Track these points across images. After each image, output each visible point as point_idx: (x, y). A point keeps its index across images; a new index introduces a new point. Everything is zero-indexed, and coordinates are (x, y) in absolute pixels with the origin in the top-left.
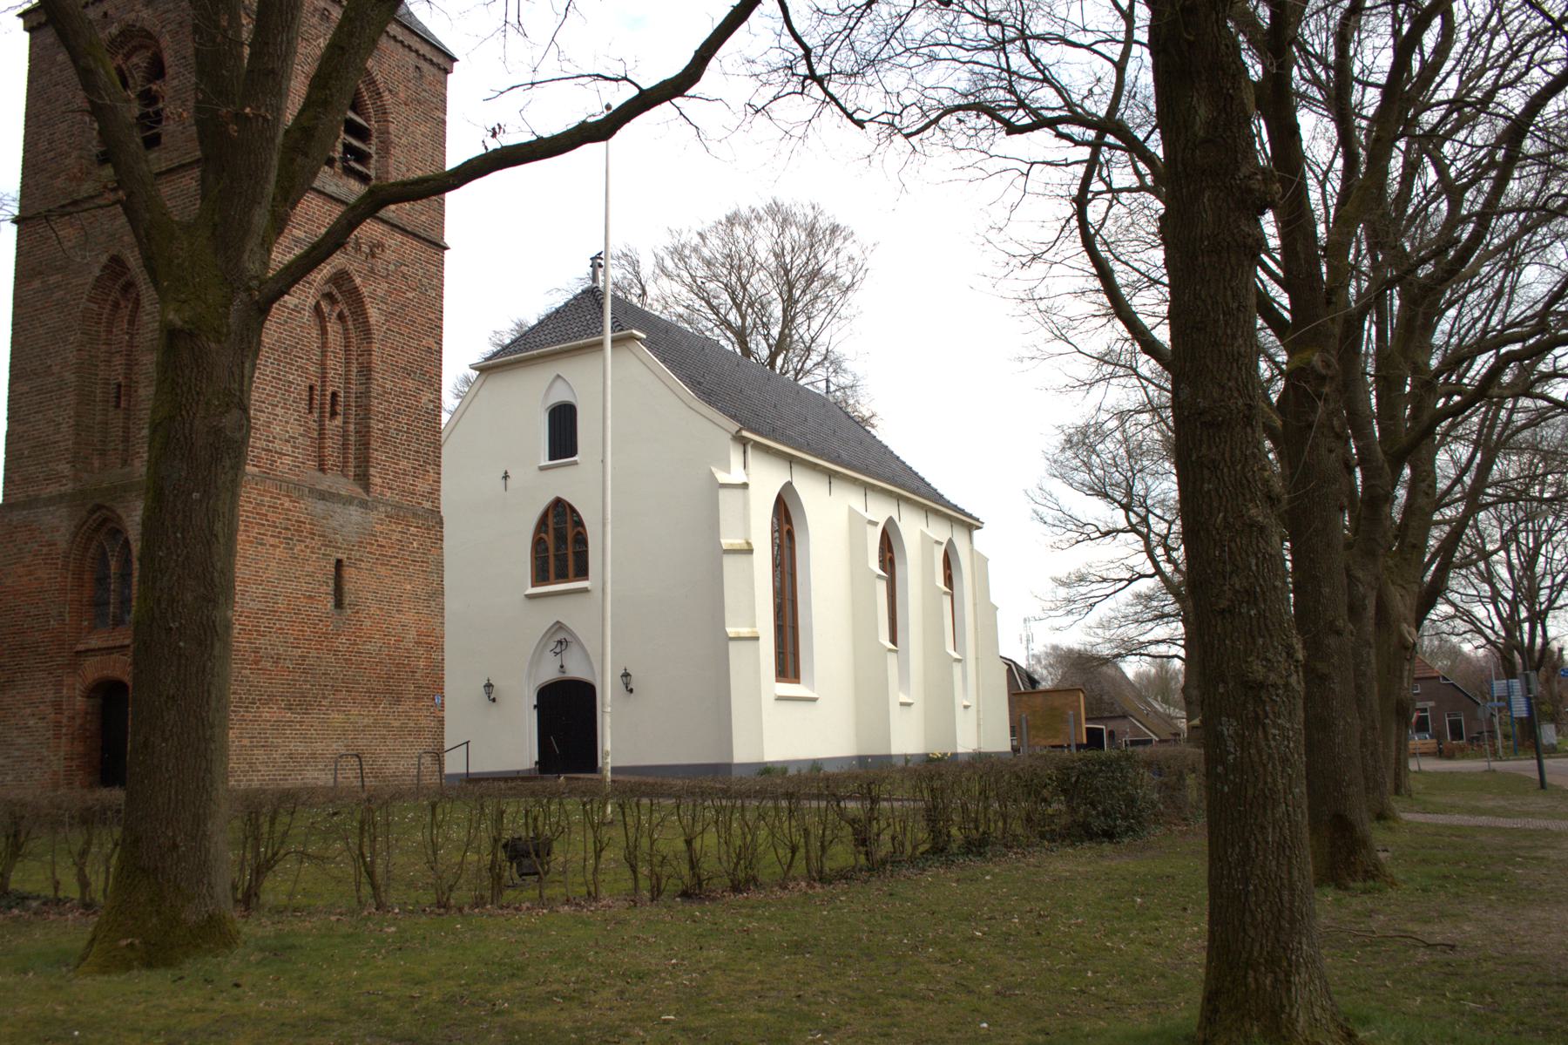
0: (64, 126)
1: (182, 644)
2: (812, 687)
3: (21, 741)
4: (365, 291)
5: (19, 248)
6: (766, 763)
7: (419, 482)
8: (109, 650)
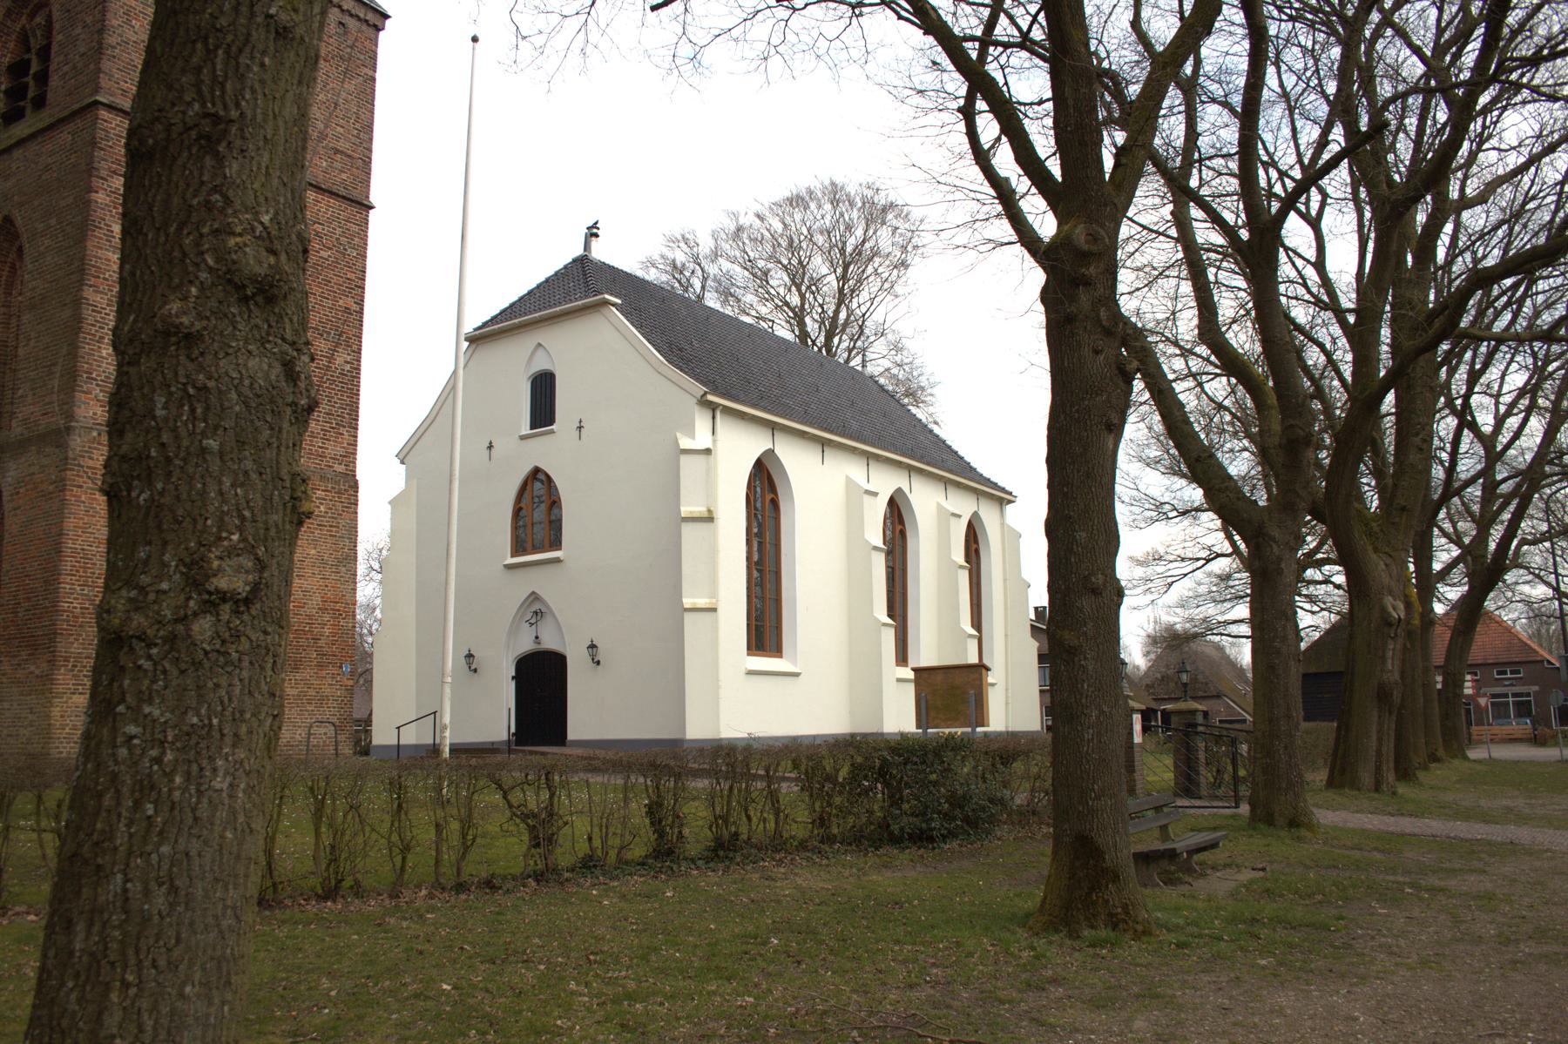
2: (794, 662)
6: (721, 739)
7: (330, 446)
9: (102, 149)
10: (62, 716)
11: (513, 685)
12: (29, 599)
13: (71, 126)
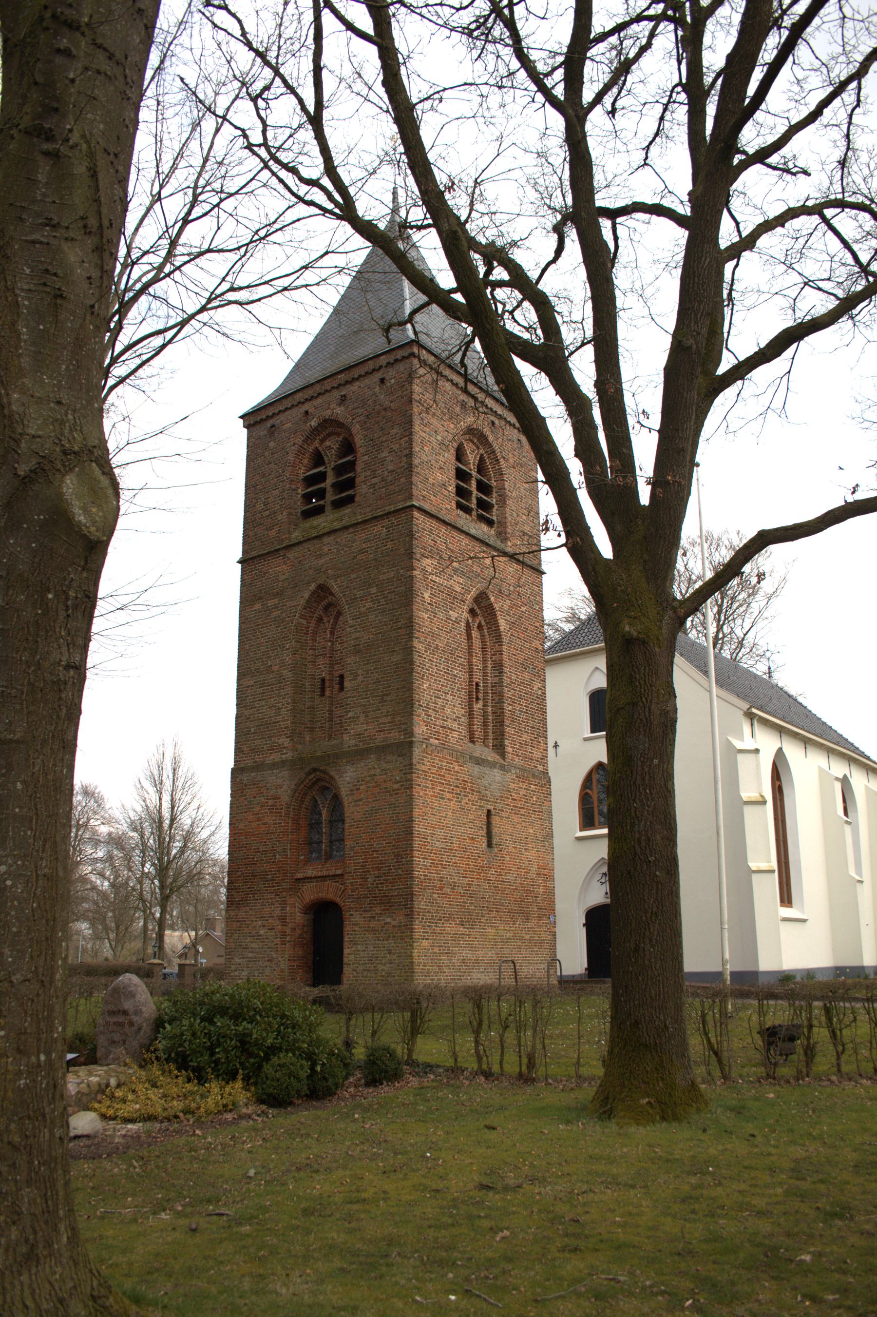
0: (276, 492)
1: (658, 873)
2: (802, 910)
3: (253, 945)
4: (496, 606)
5: (243, 580)
6: (784, 971)
8: (324, 878)
11: (584, 930)
12: (378, 869)
13: (386, 522)
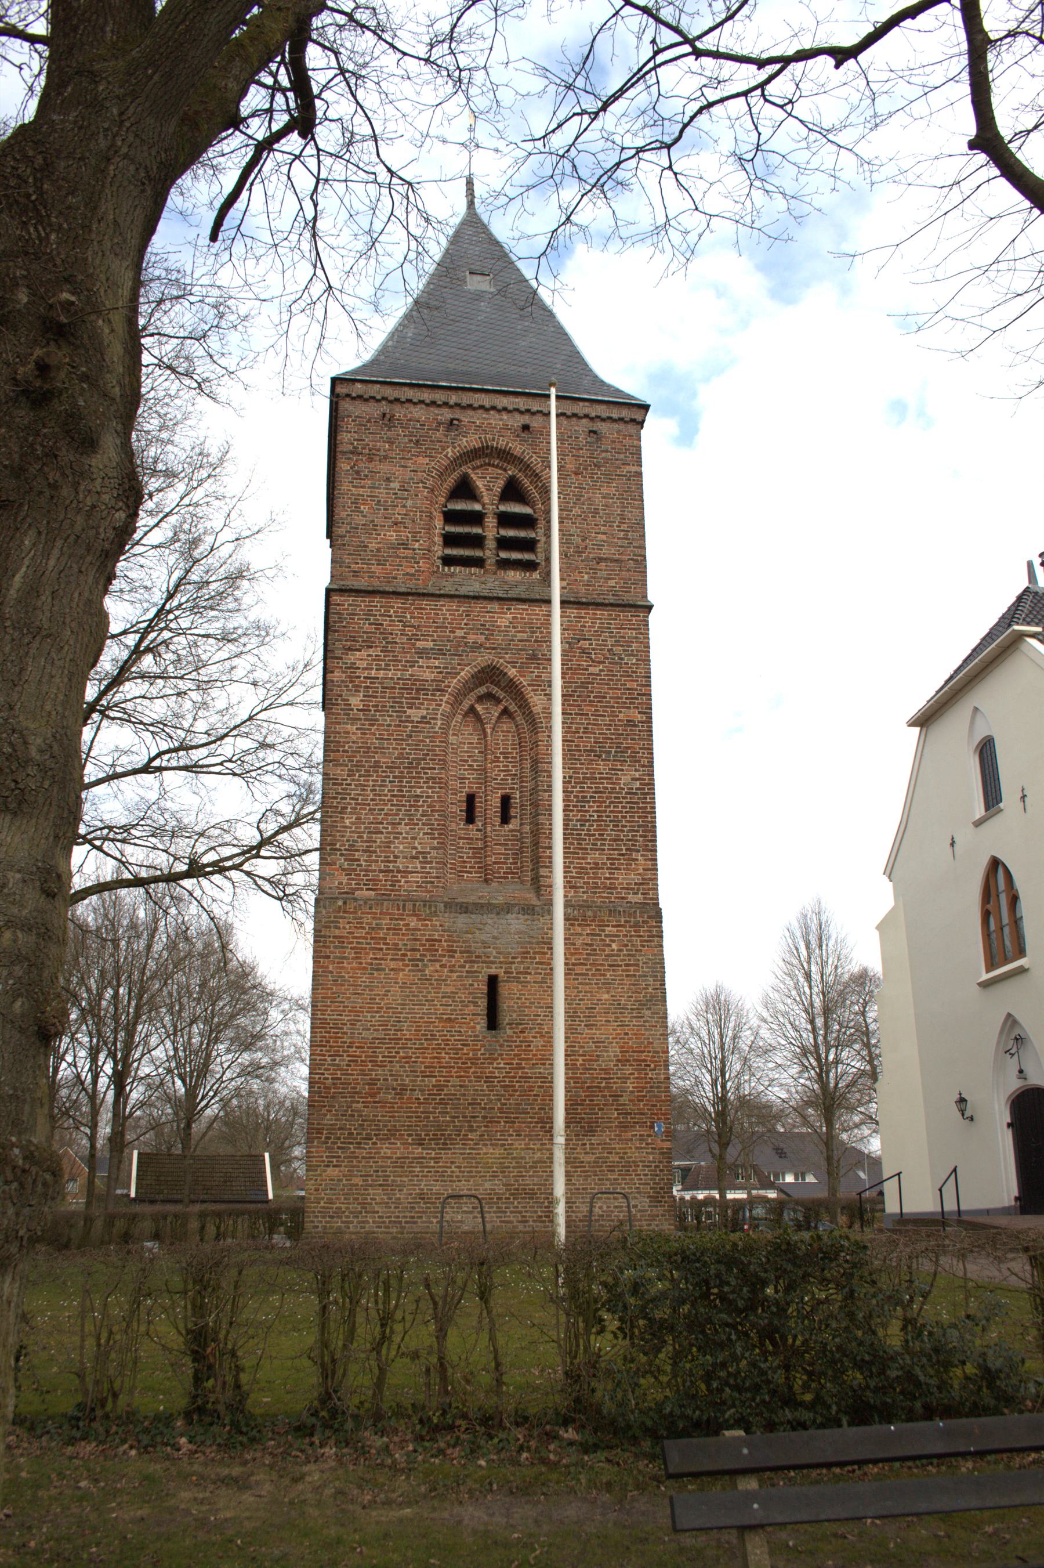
9: (336, 631)
10: (317, 1190)
